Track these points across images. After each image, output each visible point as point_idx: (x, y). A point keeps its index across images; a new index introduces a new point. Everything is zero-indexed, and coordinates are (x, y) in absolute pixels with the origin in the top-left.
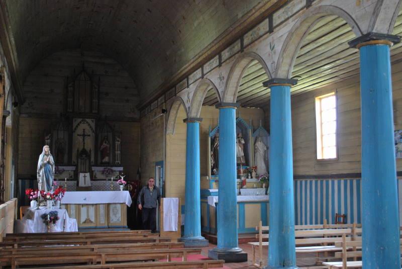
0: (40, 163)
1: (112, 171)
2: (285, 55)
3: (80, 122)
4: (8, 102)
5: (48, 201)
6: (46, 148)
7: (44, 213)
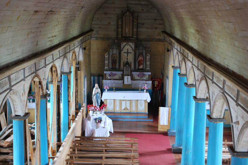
0: (94, 93)
1: (144, 75)
2: (190, 76)
3: (126, 45)
4: (80, 55)
7: (95, 118)
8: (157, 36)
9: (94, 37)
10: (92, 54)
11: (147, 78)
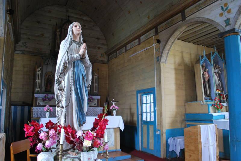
1: (93, 99)
6: (75, 28)
8: (101, 57)
9: (19, 51)
10: (14, 73)
11: (95, 104)
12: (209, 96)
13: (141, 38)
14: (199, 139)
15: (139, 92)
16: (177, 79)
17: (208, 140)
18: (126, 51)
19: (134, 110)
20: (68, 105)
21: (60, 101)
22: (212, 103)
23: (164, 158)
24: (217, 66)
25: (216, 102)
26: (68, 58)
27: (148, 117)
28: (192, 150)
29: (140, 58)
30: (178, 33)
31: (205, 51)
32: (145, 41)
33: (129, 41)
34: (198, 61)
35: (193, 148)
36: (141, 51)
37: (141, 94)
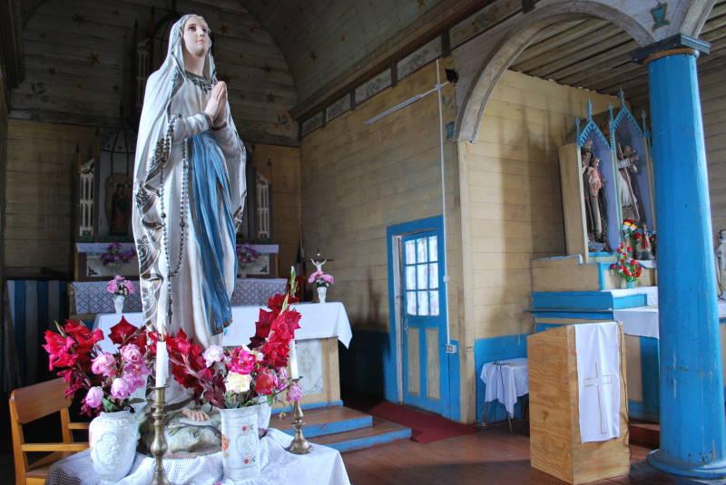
0: (151, 124)
1: (256, 255)
5: (230, 420)
6: (189, 35)
8: (276, 125)
9: (24, 110)
11: (264, 270)
12: (601, 241)
13: (401, 64)
14: (570, 364)
15: (393, 230)
16: (507, 191)
17: (597, 366)
18: (354, 106)
19: (381, 285)
20: (176, 272)
21: (152, 260)
22: (612, 259)
23: (471, 422)
24: (628, 149)
25: (622, 257)
26: (171, 127)
27: (422, 304)
28: (551, 399)
29: (395, 129)
30: (512, 51)
31: (591, 106)
32: (411, 74)
33: (361, 76)
34: (570, 136)
35: (553, 392)
36: (398, 107)
37: (400, 237)
